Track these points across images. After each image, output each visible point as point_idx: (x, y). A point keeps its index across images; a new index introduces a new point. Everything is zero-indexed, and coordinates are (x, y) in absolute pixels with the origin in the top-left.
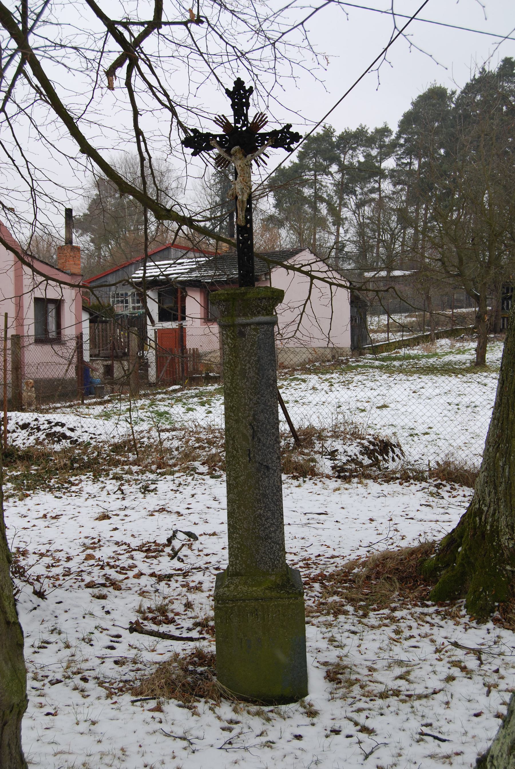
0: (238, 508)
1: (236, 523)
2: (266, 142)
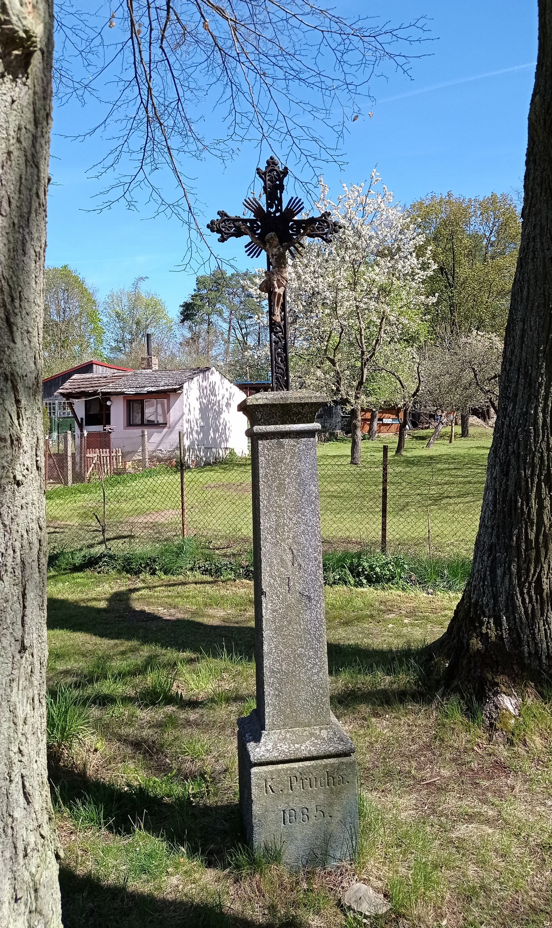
0: (276, 647)
1: (273, 665)
2: (302, 231)
